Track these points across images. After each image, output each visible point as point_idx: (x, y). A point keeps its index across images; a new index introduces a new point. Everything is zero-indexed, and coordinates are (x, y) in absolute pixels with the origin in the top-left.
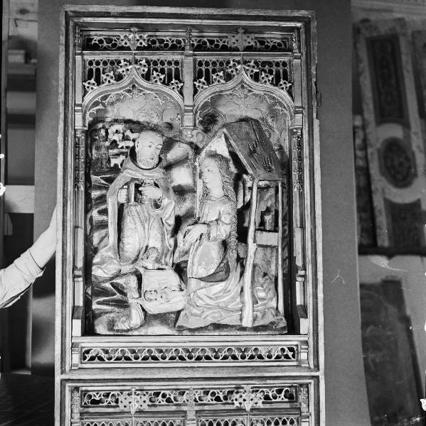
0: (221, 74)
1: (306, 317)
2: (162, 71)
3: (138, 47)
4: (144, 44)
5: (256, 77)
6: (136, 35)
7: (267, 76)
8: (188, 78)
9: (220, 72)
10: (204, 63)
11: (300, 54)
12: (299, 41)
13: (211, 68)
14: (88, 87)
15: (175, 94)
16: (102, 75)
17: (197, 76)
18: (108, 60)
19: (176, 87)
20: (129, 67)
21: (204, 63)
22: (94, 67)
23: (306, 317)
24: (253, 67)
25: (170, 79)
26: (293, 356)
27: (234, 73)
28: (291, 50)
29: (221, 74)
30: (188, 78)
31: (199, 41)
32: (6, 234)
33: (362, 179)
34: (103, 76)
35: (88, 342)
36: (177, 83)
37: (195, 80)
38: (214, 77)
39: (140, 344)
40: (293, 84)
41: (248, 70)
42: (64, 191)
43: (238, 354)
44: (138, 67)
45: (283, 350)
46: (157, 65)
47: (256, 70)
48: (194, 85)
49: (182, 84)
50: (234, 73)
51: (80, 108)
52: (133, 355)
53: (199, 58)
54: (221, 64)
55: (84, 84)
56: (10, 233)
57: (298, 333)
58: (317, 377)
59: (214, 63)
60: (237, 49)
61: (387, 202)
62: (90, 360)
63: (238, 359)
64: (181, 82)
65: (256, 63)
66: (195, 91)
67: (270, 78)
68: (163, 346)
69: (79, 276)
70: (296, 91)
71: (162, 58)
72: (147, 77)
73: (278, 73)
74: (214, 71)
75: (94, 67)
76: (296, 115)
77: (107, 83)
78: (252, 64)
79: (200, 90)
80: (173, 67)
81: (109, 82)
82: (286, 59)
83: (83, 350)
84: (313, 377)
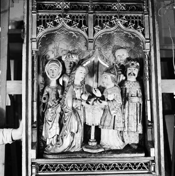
0: (52, 22)
1: (154, 147)
2: (77, 21)
3: (121, 10)
5: (126, 25)
6: (64, 3)
7: (76, 23)
8: (90, 23)
9: (51, 22)
10: (75, 17)
13: (102, 20)
14: (40, 29)
15: (84, 33)
17: (38, 24)
18: (98, 16)
20: (61, 19)
21: (75, 17)
22: (42, 19)
23: (154, 147)
24: (59, 18)
28: (142, 10)
29: (52, 22)
30: (90, 23)
31: (50, 6)
32: (7, 105)
33: (150, 75)
35: (40, 161)
36: (85, 27)
37: (94, 26)
38: (104, 25)
40: (144, 28)
41: (66, 20)
45: (60, 166)
47: (126, 21)
49: (143, 29)
50: (115, 23)
51: (35, 40)
52: (130, 166)
53: (40, 14)
54: (108, 17)
55: (38, 27)
56: (9, 104)
57: (150, 156)
59: (104, 17)
63: (105, 170)
66: (94, 32)
67: (133, 25)
68: (121, 162)
69: (35, 127)
70: (147, 32)
72: (70, 24)
73: (81, 21)
74: (48, 21)
75: (42, 19)
76: (146, 43)
77: (49, 27)
78: (68, 16)
79: (96, 31)
81: (51, 26)
82: (140, 15)
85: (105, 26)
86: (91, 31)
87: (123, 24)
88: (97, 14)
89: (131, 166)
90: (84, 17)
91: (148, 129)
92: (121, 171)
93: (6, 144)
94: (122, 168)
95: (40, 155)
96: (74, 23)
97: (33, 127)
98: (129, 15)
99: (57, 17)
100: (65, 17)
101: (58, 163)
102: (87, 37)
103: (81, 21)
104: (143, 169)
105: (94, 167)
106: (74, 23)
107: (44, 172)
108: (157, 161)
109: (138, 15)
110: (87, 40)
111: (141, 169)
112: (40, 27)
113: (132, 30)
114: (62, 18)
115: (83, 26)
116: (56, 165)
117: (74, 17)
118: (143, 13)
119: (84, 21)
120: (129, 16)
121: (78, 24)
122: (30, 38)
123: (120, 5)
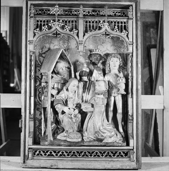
0: (46, 26)
11: (132, 18)
13: (43, 24)
14: (36, 32)
16: (42, 27)
18: (123, 21)
19: (38, 32)
20: (54, 23)
21: (123, 22)
25: (72, 29)
27: (102, 26)
34: (43, 28)
37: (34, 30)
39: (72, 159)
40: (78, 30)
46: (73, 22)
48: (34, 32)
53: (37, 19)
54: (96, 22)
60: (105, 16)
61: (106, 133)
62: (83, 152)
65: (63, 21)
70: (130, 36)
71: (119, 20)
78: (61, 21)
80: (123, 25)
88: (87, 20)
89: (100, 155)
90: (125, 23)
91: (129, 123)
92: (79, 158)
94: (91, 156)
95: (36, 141)
97: (30, 118)
98: (66, 19)
99: (52, 21)
100: (59, 22)
103: (122, 26)
104: (121, 157)
105: (97, 155)
106: (66, 27)
107: (72, 158)
109: (117, 20)
110: (77, 43)
112: (36, 30)
115: (74, 30)
116: (106, 156)
117: (66, 22)
118: (128, 19)
119: (125, 26)
120: (118, 21)
122: (28, 40)
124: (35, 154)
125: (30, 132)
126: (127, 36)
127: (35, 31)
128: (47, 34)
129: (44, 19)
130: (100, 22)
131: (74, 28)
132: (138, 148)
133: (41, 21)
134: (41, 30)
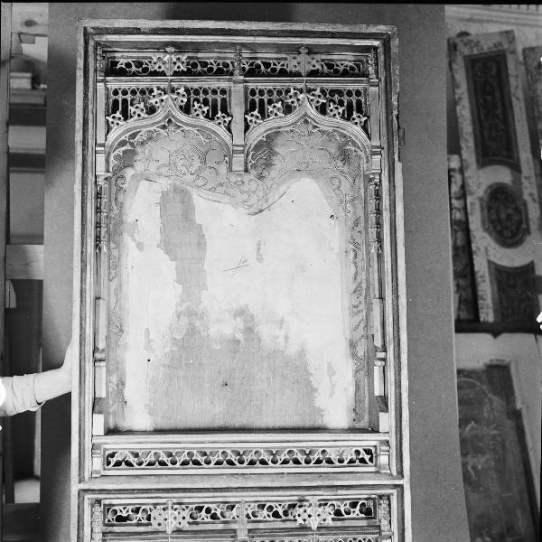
0: (279, 105)
1: (386, 409)
2: (206, 102)
4: (182, 68)
5: (322, 110)
7: (337, 108)
8: (237, 110)
10: (257, 91)
12: (377, 64)
13: (266, 98)
14: (251, 121)
15: (222, 131)
16: (130, 107)
20: (164, 97)
22: (120, 97)
24: (319, 96)
26: (371, 460)
29: (279, 105)
30: (237, 110)
34: (132, 109)
36: (224, 117)
38: (271, 109)
40: (369, 117)
41: (312, 100)
42: (82, 319)
43: (301, 458)
44: (174, 96)
46: (199, 94)
48: (246, 119)
49: (230, 118)
53: (251, 86)
54: (279, 93)
55: (107, 118)
58: (401, 487)
59: (270, 92)
62: (115, 465)
64: (228, 115)
65: (323, 91)
66: (247, 127)
70: (373, 127)
71: (205, 85)
73: (350, 104)
74: (270, 102)
75: (120, 97)
77: (136, 117)
78: (318, 92)
79: (252, 125)
80: (354, 99)
81: (139, 115)
83: (107, 453)
84: (395, 486)
85: (134, 113)
86: (238, 126)
87: (317, 108)
93: (49, 402)
96: (332, 107)
101: (185, 448)
102: (227, 138)
108: (393, 443)
111: (355, 462)
112: (252, 115)
113: (202, 120)
114: (167, 96)
115: (219, 114)
121: (343, 108)
123: (175, 60)
124: (109, 463)
125: (95, 398)
126: (229, 129)
127: (110, 119)
128: (280, 128)
129: (270, 86)
130: (288, 91)
131: (219, 107)
132: (396, 411)
133: (261, 92)
134: (263, 114)
